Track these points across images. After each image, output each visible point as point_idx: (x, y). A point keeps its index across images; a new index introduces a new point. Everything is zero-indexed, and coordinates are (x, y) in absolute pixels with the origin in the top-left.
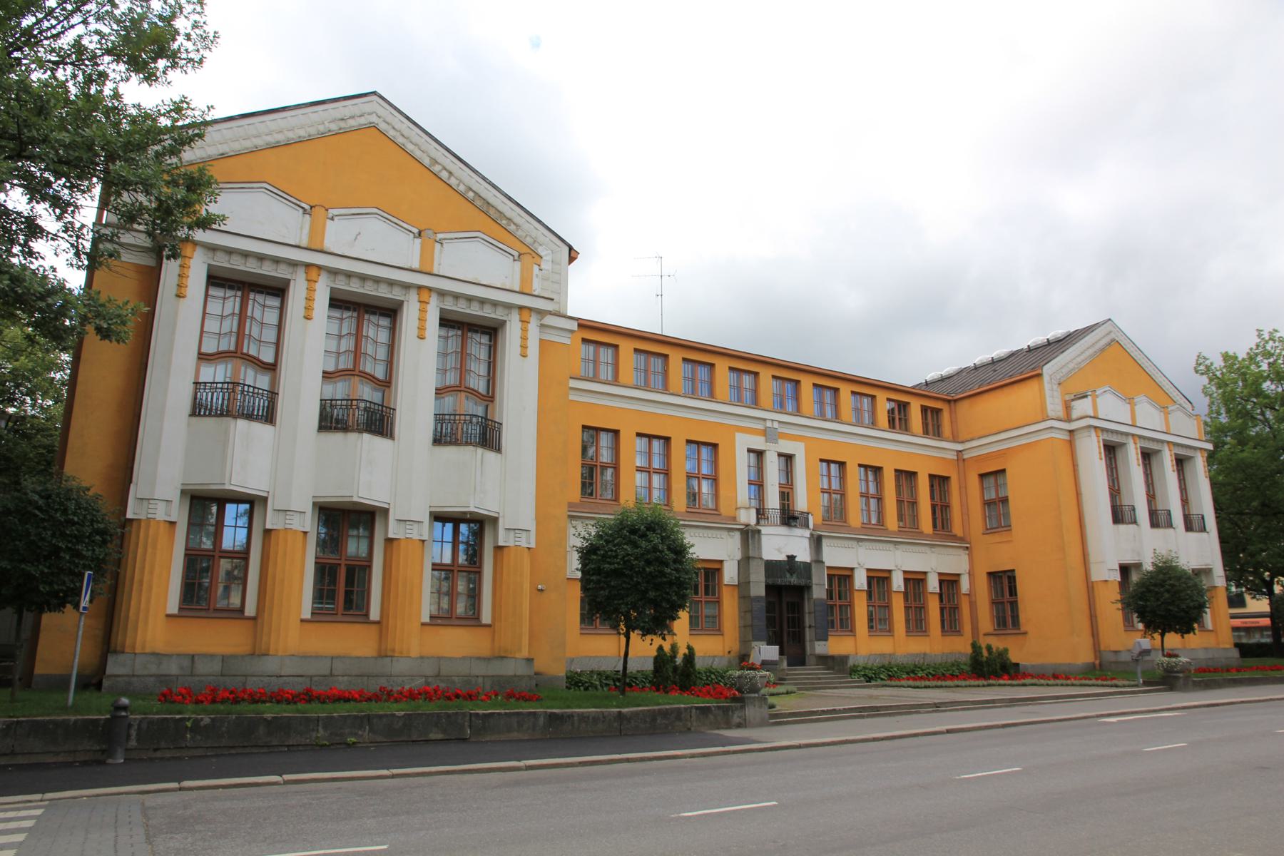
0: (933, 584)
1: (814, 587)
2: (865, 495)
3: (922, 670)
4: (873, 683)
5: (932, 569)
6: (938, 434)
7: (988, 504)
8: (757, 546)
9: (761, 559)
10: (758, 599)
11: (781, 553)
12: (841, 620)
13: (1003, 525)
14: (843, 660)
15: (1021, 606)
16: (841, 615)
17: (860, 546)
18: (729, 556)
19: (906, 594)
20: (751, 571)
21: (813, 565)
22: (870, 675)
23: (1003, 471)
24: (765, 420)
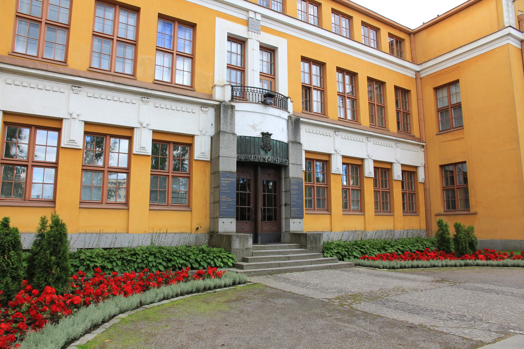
0: (397, 173)
1: (291, 166)
2: (342, 96)
3: (392, 246)
4: (346, 262)
5: (397, 161)
6: (400, 55)
7: (442, 111)
8: (229, 121)
9: (234, 134)
10: (228, 174)
11: (256, 130)
12: (318, 200)
13: (454, 127)
14: (317, 237)
15: (471, 192)
16: (318, 195)
17: (338, 135)
18: (201, 132)
19: (375, 180)
20: (221, 145)
21: (290, 145)
22: (343, 253)
23: (457, 81)
24: (247, 11)
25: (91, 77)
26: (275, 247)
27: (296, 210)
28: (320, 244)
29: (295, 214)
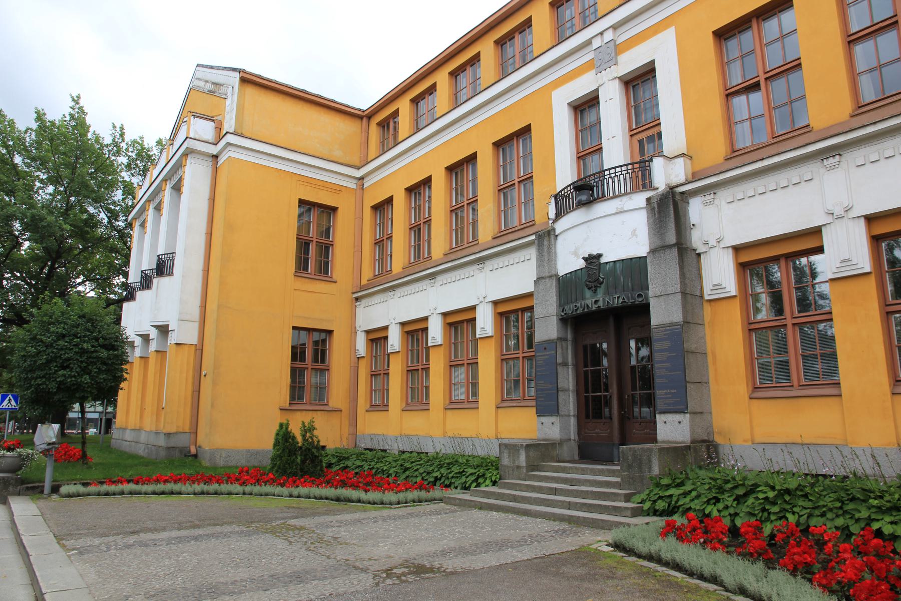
1: (652, 302)
24: (589, 42)
25: (501, 243)
26: (583, 469)
27: (666, 394)
28: (650, 472)
29: (665, 404)
